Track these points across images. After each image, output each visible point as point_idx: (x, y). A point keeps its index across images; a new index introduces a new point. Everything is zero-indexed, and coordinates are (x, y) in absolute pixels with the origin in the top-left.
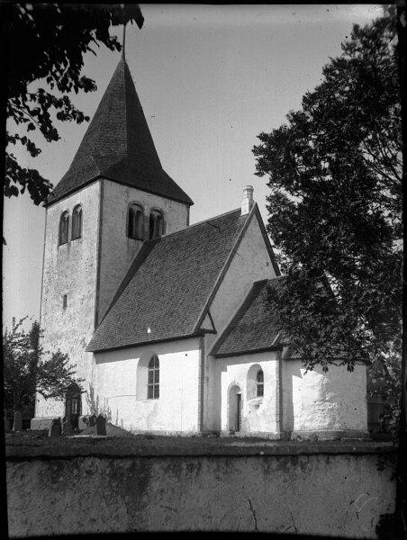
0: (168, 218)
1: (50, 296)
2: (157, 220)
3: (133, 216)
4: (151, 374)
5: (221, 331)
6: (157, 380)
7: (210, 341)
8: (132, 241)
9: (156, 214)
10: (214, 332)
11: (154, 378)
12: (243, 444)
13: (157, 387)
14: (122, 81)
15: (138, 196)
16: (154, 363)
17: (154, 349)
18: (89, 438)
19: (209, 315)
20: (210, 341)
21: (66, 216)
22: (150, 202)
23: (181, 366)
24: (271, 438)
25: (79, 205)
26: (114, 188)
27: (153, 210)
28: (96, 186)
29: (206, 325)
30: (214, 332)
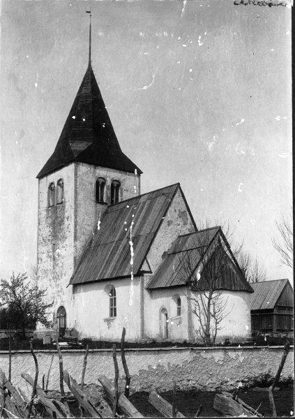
0: (124, 186)
1: (44, 256)
2: (116, 186)
3: (100, 184)
4: (111, 300)
5: (154, 270)
6: (115, 305)
7: (147, 278)
8: (98, 205)
9: (116, 183)
10: (151, 272)
11: (113, 302)
12: (135, 349)
13: (115, 309)
14: (87, 91)
15: (102, 172)
16: (113, 292)
17: (113, 283)
18: (133, 246)
19: (147, 262)
20: (147, 278)
21: (53, 186)
22: (110, 175)
23: (129, 293)
24: (174, 342)
25: (61, 180)
26: (84, 168)
27: (113, 181)
28: (72, 166)
29: (145, 268)
30: (151, 272)
